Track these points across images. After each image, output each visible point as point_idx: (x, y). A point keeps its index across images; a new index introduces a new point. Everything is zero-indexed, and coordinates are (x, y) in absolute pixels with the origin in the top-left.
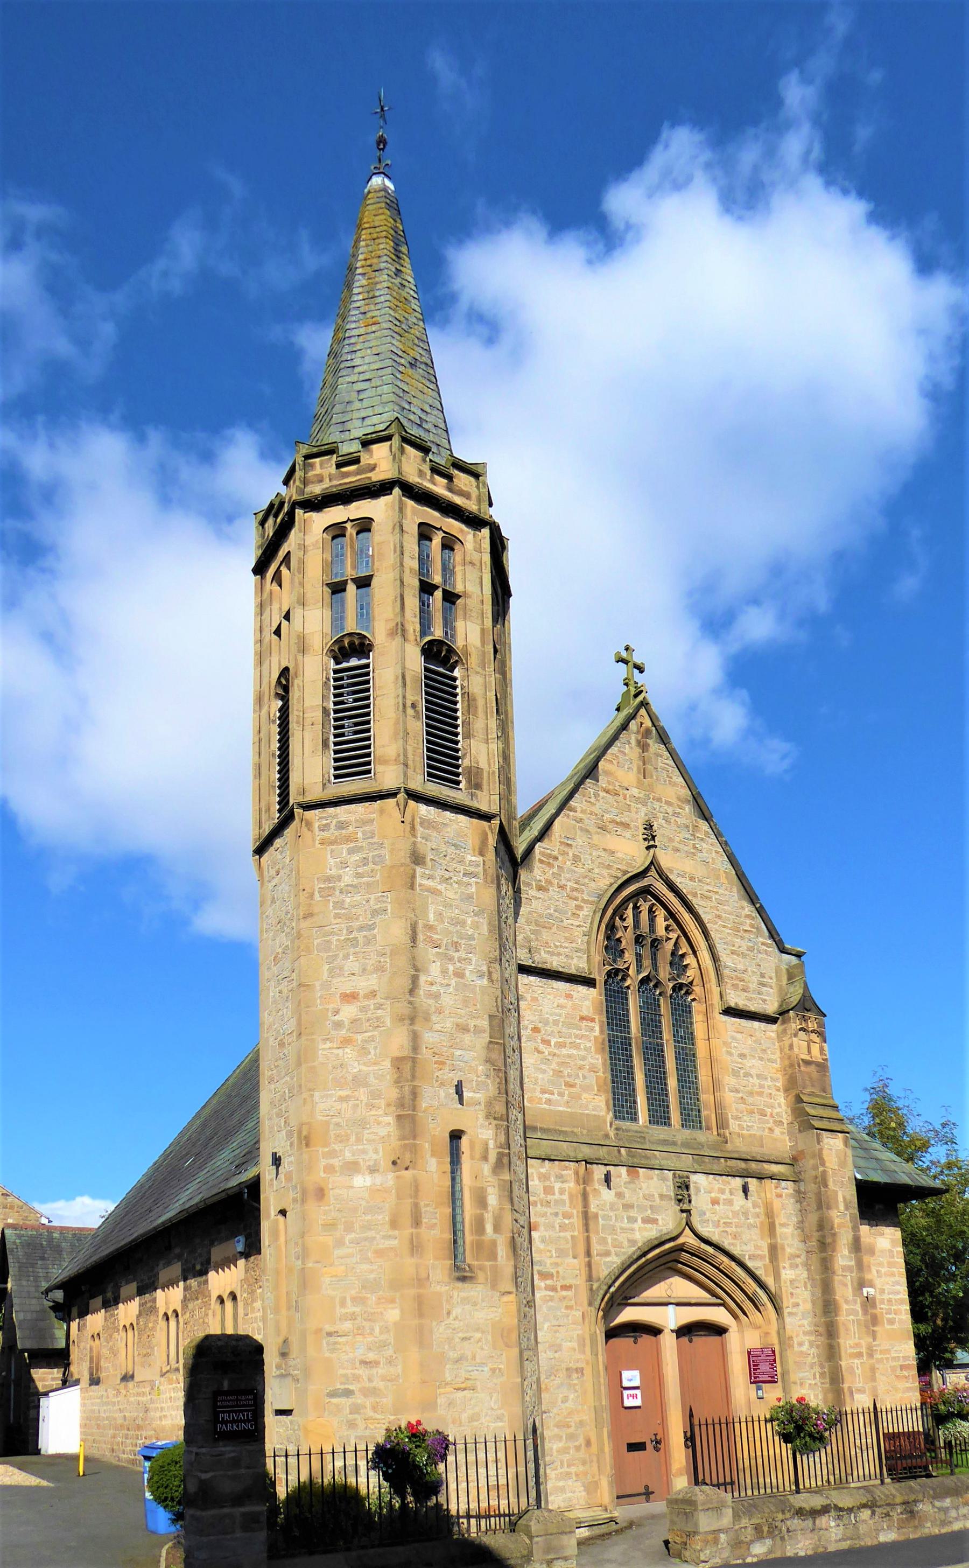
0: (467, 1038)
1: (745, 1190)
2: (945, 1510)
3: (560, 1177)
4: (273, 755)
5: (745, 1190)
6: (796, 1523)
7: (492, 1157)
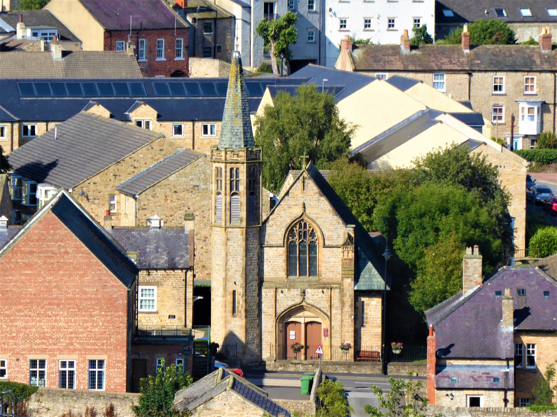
0: (237, 273)
1: (323, 292)
2: (337, 368)
3: (270, 292)
4: (190, 217)
5: (323, 292)
6: (291, 365)
7: (241, 295)
